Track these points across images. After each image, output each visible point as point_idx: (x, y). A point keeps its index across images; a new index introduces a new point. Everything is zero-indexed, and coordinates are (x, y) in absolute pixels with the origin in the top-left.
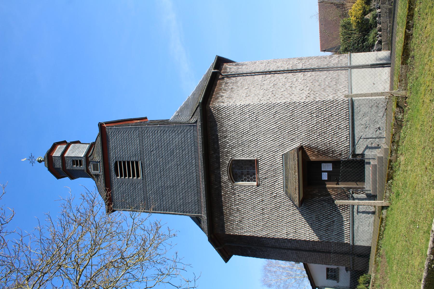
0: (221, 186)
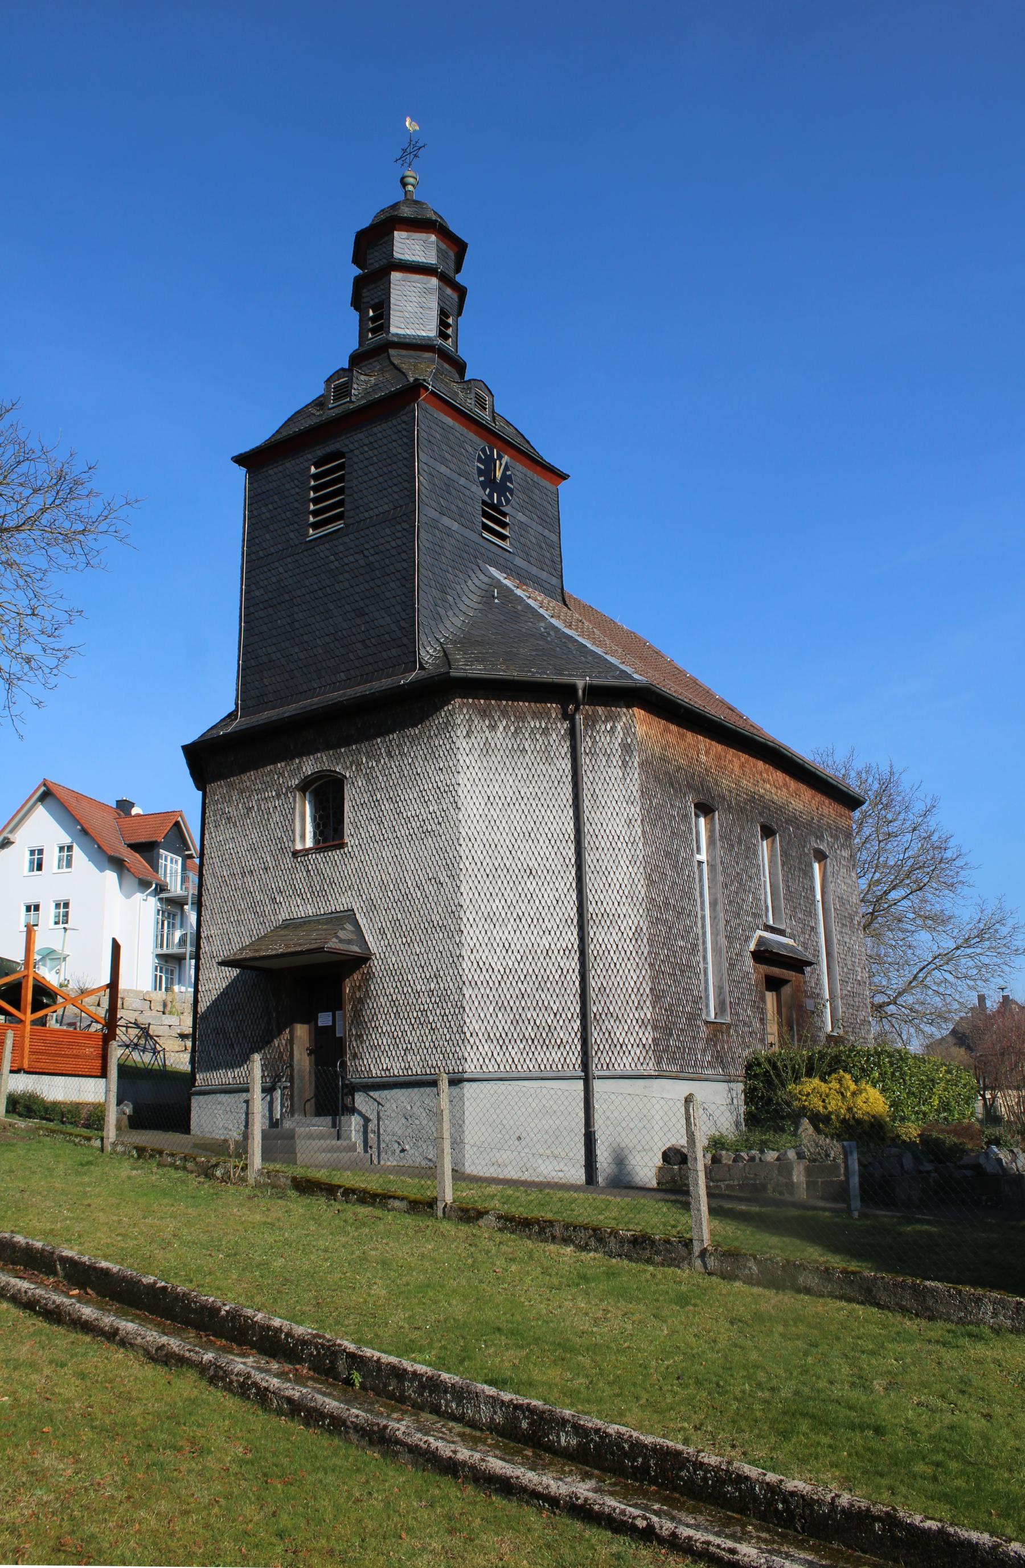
0: (293, 758)
